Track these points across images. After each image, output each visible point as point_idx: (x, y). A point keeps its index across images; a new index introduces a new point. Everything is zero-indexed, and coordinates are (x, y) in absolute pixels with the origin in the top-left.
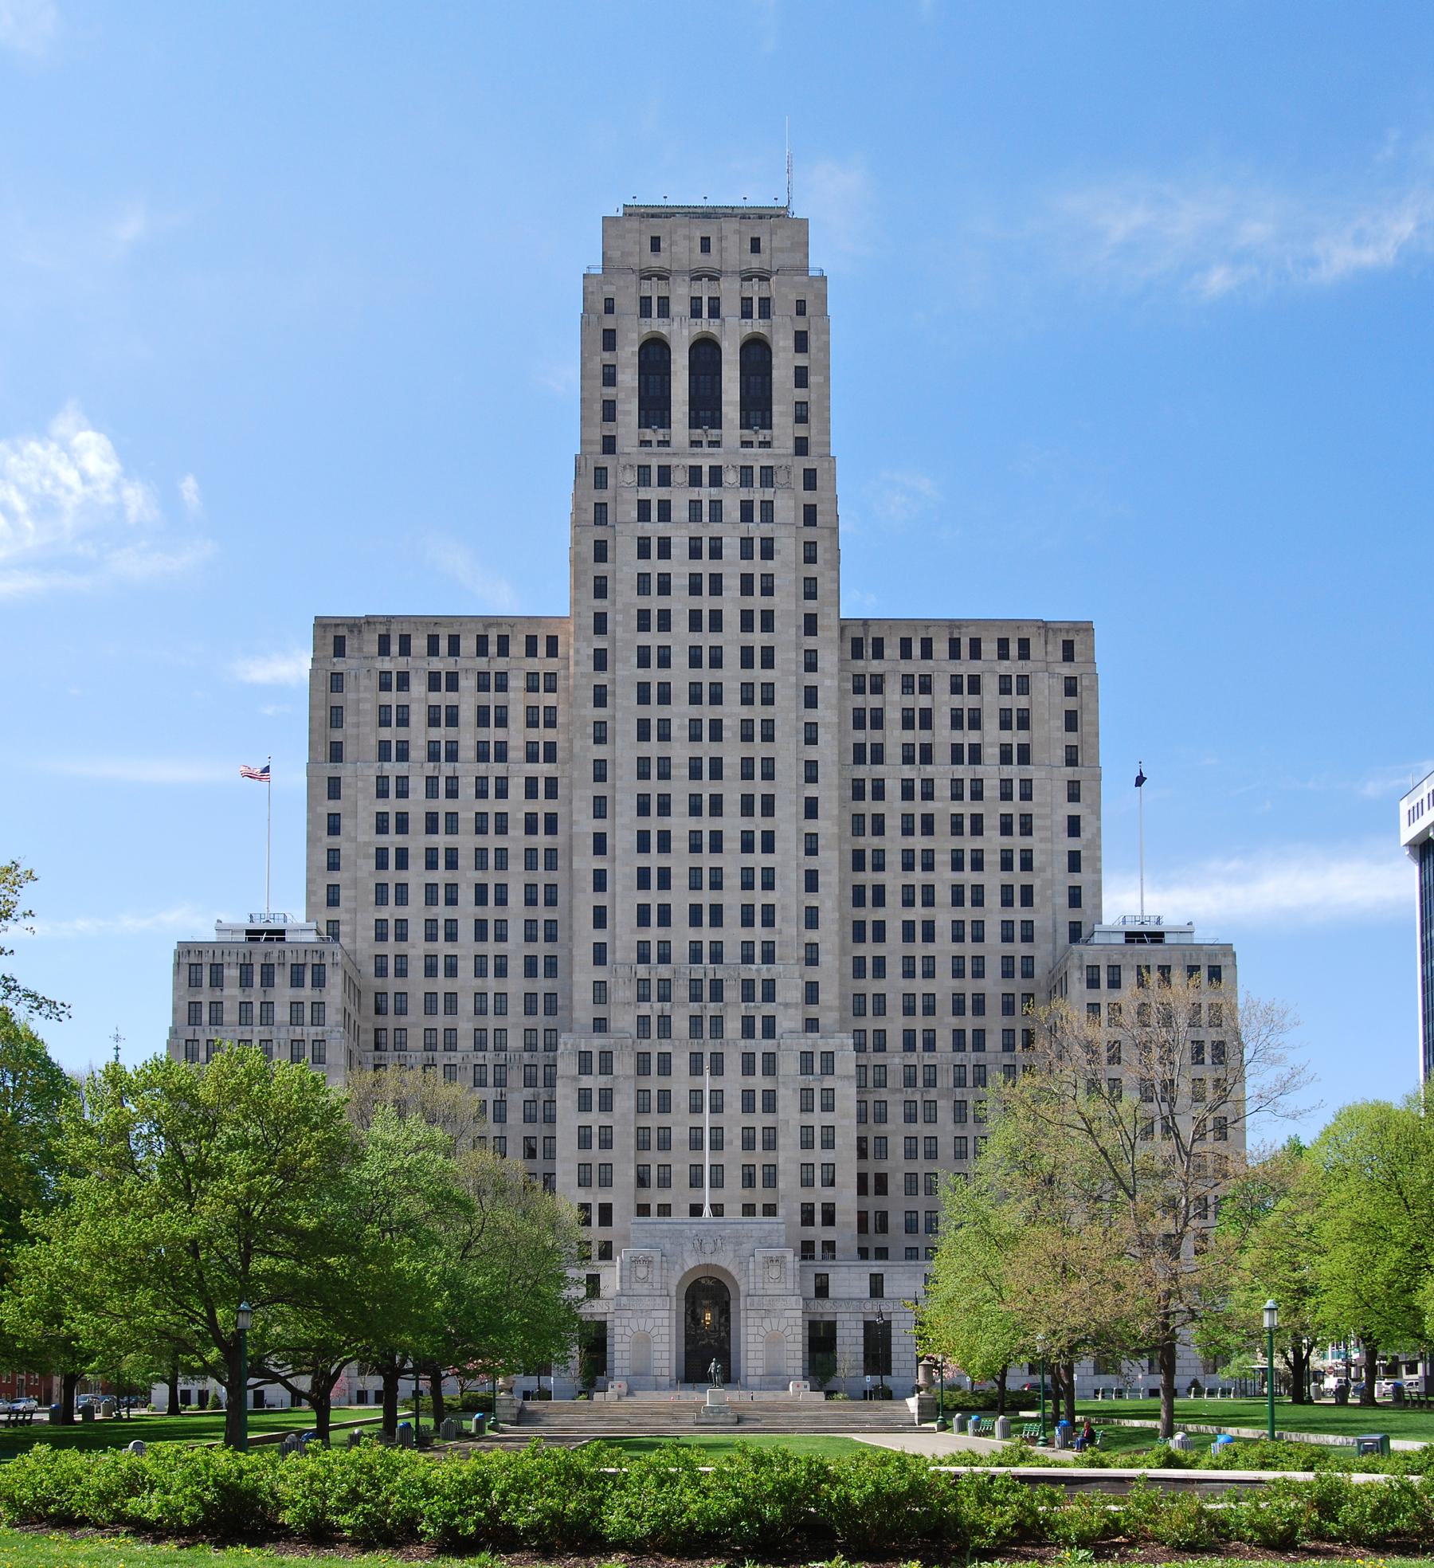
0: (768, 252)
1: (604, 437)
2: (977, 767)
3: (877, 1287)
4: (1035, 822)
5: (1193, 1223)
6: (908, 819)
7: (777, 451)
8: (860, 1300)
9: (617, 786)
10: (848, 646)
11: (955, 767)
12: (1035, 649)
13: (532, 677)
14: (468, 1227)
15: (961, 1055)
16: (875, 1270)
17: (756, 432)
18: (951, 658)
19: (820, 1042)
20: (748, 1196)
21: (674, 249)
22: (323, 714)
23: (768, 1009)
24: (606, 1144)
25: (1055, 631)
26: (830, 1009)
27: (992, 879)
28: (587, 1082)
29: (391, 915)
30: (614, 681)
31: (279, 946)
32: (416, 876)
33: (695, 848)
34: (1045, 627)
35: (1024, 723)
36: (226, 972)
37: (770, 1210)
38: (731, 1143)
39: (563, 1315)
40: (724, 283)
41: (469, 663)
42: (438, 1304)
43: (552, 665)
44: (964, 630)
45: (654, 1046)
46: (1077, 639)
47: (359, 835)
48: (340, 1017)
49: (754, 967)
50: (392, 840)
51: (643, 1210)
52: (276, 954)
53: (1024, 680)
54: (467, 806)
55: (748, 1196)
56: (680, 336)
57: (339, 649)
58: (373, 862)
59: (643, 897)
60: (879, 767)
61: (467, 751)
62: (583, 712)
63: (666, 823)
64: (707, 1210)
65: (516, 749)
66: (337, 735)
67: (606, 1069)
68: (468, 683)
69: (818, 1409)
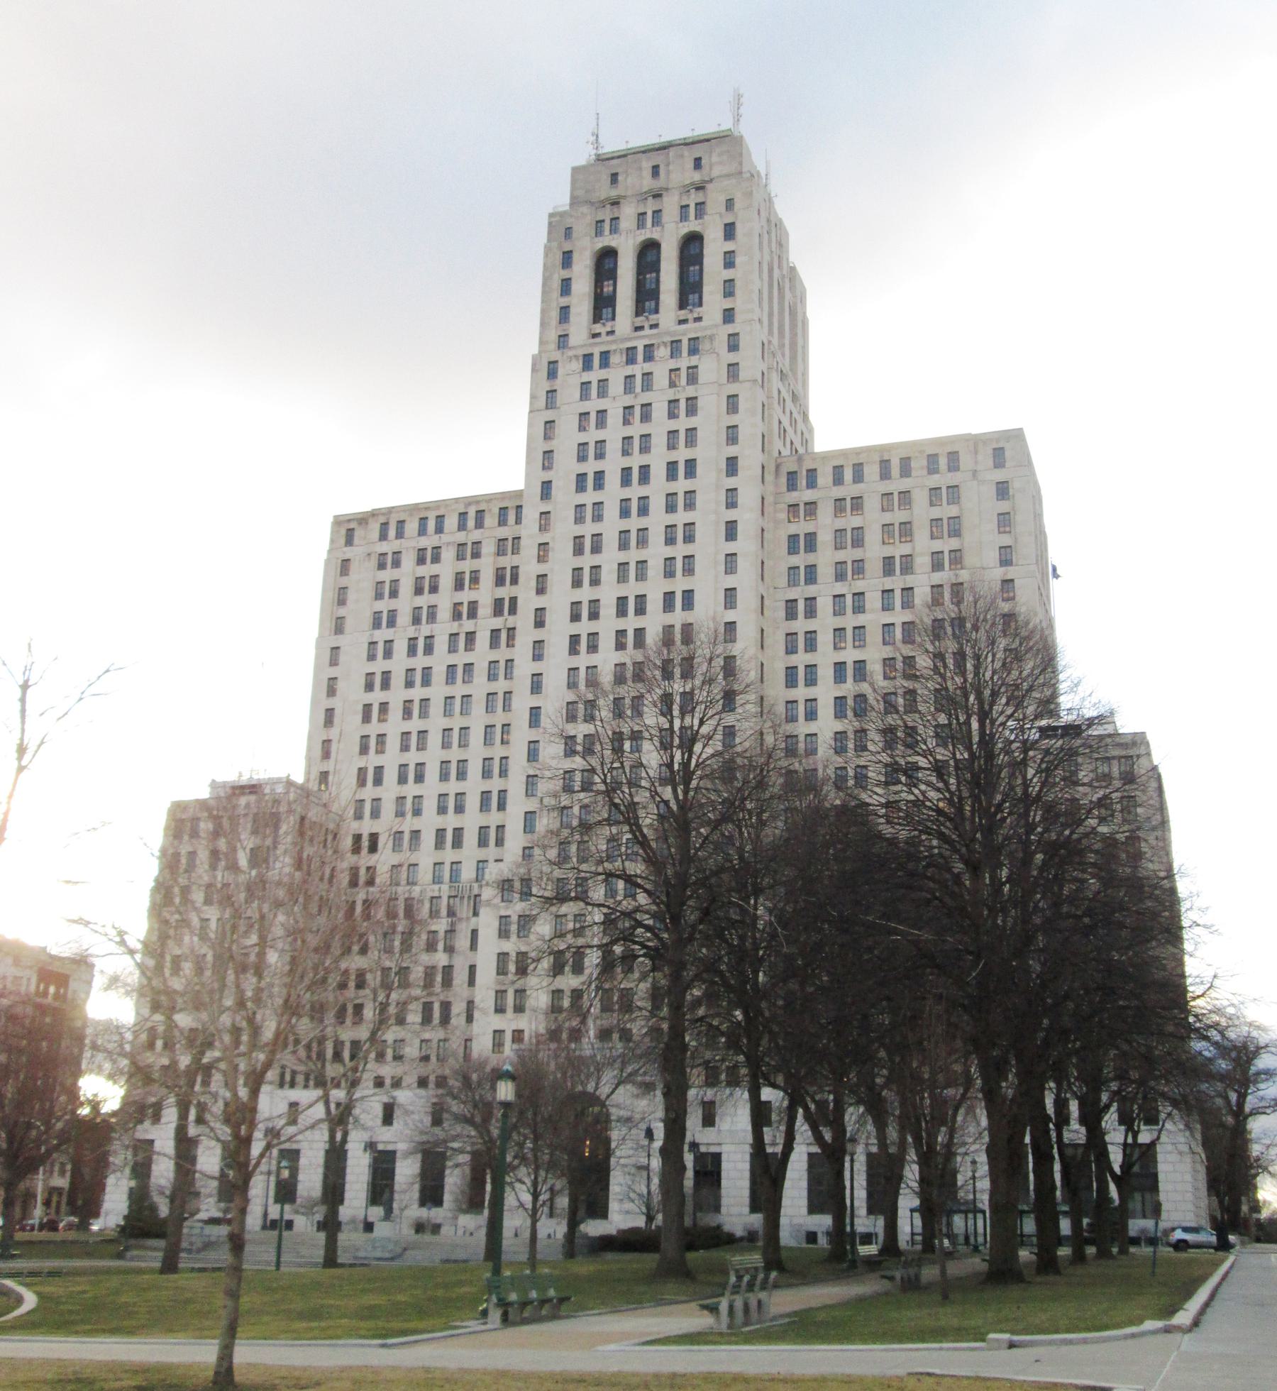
5: (363, 1033)
9: (644, 1218)
10: (783, 480)
12: (965, 461)
17: (691, 311)
18: (882, 479)
22: (333, 595)
25: (984, 443)
30: (553, 538)
34: (975, 442)
35: (956, 533)
41: (452, 535)
46: (1007, 446)
47: (352, 695)
57: (349, 541)
64: (433, 1059)
66: (342, 612)
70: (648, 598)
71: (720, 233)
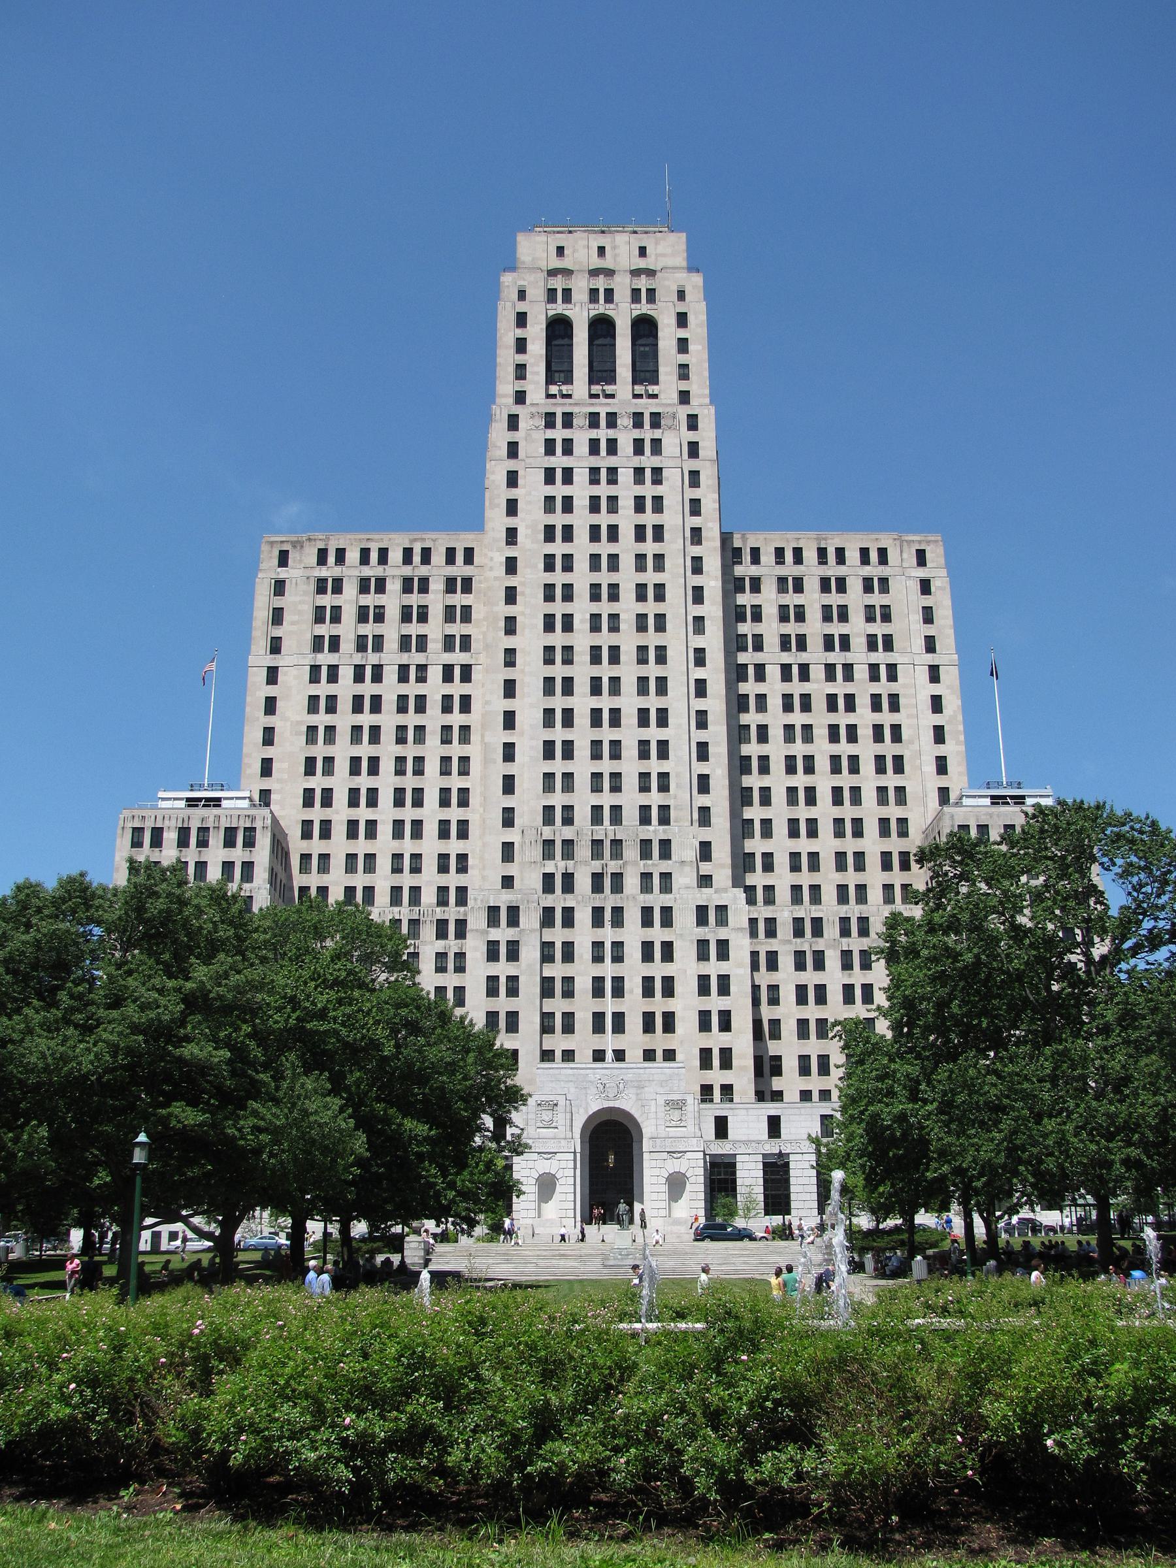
0: (653, 257)
1: (794, 919)
2: (847, 654)
3: (774, 1126)
4: (902, 701)
6: (596, 745)
7: (664, 401)
8: (758, 1142)
11: (828, 654)
12: (892, 556)
13: (782, 581)
14: (275, 1555)
15: (845, 907)
16: (773, 1113)
19: (715, 896)
20: (648, 1041)
21: (576, 255)
23: (665, 866)
24: (513, 991)
26: (722, 866)
27: (866, 749)
28: (495, 934)
29: (319, 784)
31: (216, 811)
32: (344, 720)
33: (618, 912)
35: (887, 617)
36: (165, 835)
37: (670, 1055)
38: (631, 992)
39: (368, 980)
40: (617, 278)
42: (20, 1208)
43: (468, 571)
44: (829, 541)
45: (558, 900)
48: (266, 875)
49: (650, 828)
50: (322, 719)
51: (547, 1055)
52: (212, 819)
53: (884, 581)
54: (390, 688)
55: (648, 1041)
56: (580, 315)
58: (469, 927)
59: (659, 490)
60: (760, 654)
61: (581, 476)
62: (496, 609)
63: (597, 1005)
65: (435, 641)
67: (513, 921)
68: (394, 586)
69: (928, 542)
70: (621, 649)
71: (673, 321)
